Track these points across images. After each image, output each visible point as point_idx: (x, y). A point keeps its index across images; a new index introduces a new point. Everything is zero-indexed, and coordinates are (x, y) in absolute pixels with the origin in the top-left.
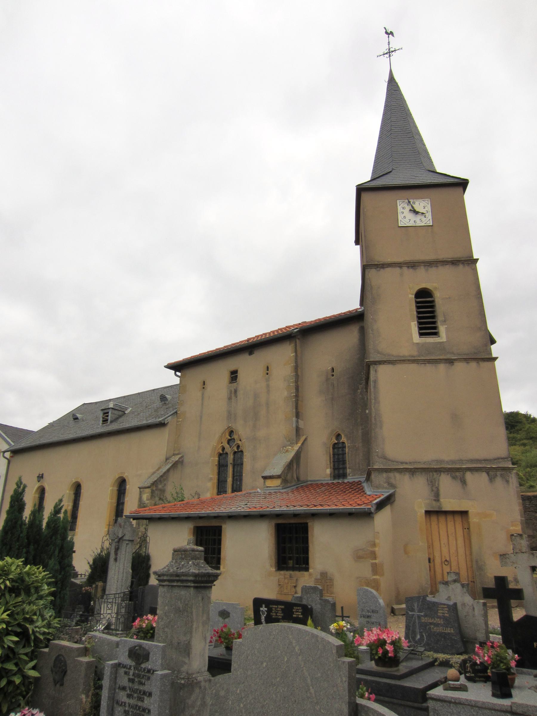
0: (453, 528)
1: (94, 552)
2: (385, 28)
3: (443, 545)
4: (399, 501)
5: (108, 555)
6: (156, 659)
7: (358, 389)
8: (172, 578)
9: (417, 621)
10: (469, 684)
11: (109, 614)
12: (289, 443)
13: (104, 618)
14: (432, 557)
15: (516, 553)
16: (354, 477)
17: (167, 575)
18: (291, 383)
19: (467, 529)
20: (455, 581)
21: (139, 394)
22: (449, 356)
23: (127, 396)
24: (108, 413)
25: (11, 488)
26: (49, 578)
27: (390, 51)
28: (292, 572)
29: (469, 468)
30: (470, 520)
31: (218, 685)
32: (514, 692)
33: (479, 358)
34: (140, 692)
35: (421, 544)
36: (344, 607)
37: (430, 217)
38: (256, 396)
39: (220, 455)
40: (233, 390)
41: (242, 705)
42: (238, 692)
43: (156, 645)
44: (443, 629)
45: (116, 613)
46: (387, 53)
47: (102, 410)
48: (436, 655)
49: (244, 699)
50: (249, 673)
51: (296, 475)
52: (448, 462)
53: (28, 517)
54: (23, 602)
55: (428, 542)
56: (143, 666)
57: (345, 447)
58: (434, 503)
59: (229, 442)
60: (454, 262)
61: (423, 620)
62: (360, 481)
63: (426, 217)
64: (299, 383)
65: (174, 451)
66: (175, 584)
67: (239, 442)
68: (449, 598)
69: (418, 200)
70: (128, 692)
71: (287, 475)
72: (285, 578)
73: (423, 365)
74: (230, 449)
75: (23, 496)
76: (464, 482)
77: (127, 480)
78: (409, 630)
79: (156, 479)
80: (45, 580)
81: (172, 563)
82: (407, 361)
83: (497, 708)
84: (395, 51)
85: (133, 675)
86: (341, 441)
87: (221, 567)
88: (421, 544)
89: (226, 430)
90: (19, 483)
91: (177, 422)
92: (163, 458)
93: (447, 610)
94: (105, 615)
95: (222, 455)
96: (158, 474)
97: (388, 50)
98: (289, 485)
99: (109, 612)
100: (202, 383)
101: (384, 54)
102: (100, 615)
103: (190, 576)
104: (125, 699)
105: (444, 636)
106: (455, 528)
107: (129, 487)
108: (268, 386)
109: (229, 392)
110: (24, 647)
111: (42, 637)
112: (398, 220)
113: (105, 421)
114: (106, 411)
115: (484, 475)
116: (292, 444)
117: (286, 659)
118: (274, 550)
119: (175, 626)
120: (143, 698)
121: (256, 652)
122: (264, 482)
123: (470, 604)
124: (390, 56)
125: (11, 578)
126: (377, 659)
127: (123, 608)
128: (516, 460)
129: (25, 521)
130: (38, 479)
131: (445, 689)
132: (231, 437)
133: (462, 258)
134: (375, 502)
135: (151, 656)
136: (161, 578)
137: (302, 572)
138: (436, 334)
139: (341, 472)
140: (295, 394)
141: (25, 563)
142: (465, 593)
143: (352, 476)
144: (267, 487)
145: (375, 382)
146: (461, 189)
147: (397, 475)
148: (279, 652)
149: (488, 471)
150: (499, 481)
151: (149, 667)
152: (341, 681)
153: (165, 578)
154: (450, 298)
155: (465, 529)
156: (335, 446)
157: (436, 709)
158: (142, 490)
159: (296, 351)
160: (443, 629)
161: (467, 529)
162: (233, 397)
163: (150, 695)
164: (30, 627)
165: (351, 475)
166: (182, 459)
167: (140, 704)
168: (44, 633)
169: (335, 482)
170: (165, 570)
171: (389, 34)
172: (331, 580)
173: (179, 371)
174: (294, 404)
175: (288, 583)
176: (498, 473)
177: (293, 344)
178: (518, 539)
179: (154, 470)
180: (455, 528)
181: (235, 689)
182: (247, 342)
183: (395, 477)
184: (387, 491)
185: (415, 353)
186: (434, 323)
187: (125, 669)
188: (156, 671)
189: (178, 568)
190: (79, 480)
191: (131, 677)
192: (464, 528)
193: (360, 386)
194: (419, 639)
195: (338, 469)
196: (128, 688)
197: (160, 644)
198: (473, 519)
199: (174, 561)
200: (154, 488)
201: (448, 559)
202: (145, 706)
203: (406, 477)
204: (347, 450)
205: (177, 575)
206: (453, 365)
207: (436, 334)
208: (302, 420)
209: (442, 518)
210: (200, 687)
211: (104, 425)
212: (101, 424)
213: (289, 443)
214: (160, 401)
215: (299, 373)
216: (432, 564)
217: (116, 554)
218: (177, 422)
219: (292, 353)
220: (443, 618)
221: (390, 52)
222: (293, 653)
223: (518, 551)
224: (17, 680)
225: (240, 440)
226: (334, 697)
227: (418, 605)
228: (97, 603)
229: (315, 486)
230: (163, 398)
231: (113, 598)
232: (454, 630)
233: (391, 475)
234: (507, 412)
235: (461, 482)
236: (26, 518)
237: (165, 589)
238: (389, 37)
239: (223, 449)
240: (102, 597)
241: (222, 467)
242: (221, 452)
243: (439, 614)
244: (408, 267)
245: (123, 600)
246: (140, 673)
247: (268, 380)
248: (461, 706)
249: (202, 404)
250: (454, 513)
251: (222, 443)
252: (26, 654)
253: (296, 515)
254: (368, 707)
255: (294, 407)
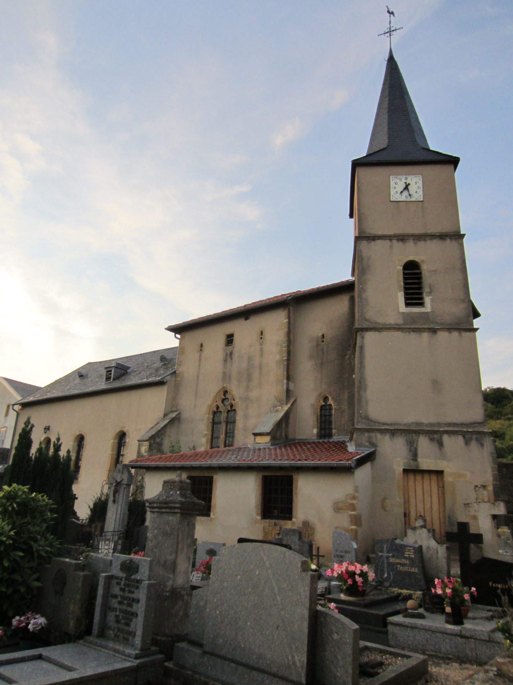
0: (429, 487)
1: (94, 497)
2: (387, 7)
3: (418, 501)
4: (379, 460)
5: (107, 501)
6: (144, 571)
7: (346, 354)
8: (161, 505)
9: (385, 561)
10: (426, 614)
11: (106, 549)
12: (279, 403)
13: (102, 553)
14: (407, 512)
15: (479, 502)
16: (339, 437)
17: (157, 503)
18: (283, 348)
19: (441, 488)
20: (422, 527)
21: (141, 355)
22: (432, 326)
23: (130, 356)
24: (111, 371)
25: (21, 426)
26: (52, 504)
27: (391, 30)
28: (276, 521)
29: (447, 431)
30: (445, 479)
31: (198, 597)
32: (465, 621)
33: (462, 329)
34: (129, 600)
35: (398, 499)
36: (320, 548)
37: (421, 193)
38: (250, 359)
39: (214, 413)
40: (229, 353)
41: (218, 612)
42: (215, 601)
43: (145, 560)
44: (408, 569)
45: (113, 549)
46: (387, 33)
47: (106, 368)
48: (400, 591)
49: (220, 607)
50: (225, 584)
51: (285, 432)
52: (427, 425)
53: (34, 454)
54: (28, 523)
55: (405, 498)
56: (133, 577)
57: (332, 409)
58: (412, 462)
59: (223, 401)
60: (442, 237)
61: (392, 560)
62: (344, 441)
63: (417, 193)
64: (291, 348)
65: (172, 408)
66: (164, 510)
67: (233, 402)
68: (416, 542)
69: (410, 176)
70: (119, 599)
71: (276, 433)
72: (269, 526)
73: (408, 333)
74: (224, 408)
75: (31, 435)
76: (441, 444)
77: (127, 434)
78: (378, 569)
79: (154, 433)
80: (49, 506)
81: (162, 493)
82: (393, 329)
83: (448, 632)
84: (396, 30)
85: (124, 585)
86: (328, 403)
87: (211, 514)
88: (398, 499)
89: (221, 389)
90: (28, 423)
91: (176, 381)
92: (161, 414)
93: (413, 552)
94: (103, 550)
95: (216, 413)
96: (156, 429)
97: (389, 29)
98: (278, 442)
99: (106, 547)
100: (200, 345)
101: (385, 33)
102: (97, 550)
103: (177, 503)
104: (116, 605)
105: (409, 574)
106: (431, 486)
107: (129, 441)
108: (261, 350)
109: (225, 355)
110: (29, 562)
111: (44, 554)
112: (390, 195)
113: (108, 378)
114: (109, 369)
115: (460, 438)
116: (281, 405)
117: (257, 573)
118: (261, 499)
119: (163, 547)
120: (132, 604)
121: (232, 567)
122: (255, 439)
123: (435, 548)
124: (390, 35)
125: (18, 502)
126: (345, 589)
127: (119, 544)
128: (500, 433)
129: (32, 457)
130: (44, 431)
131: (405, 616)
132: (225, 396)
133: (450, 233)
134: (355, 458)
135: (140, 569)
136: (152, 505)
137: (285, 521)
138: (422, 304)
139: (327, 431)
140: (286, 358)
141: (32, 491)
142: (431, 537)
143: (337, 436)
144: (257, 443)
145: (362, 348)
146: (452, 167)
147: (379, 436)
148: (252, 566)
149: (464, 434)
150: (474, 444)
151: (138, 578)
152: (304, 591)
153: (155, 505)
154: (436, 271)
155: (440, 487)
156: (322, 408)
157: (395, 632)
158: (140, 443)
159: (289, 318)
160: (408, 569)
161: (442, 487)
162: (229, 360)
163: (138, 601)
164: (35, 546)
165: (336, 435)
166: (179, 416)
167: (129, 609)
168: (47, 552)
169: (321, 441)
170: (156, 498)
171: (391, 13)
172: (313, 529)
173: (179, 334)
174: (286, 367)
175: (272, 530)
176: (474, 437)
177: (286, 312)
178: (481, 490)
179: (153, 425)
180: (431, 486)
181: (212, 599)
182: (243, 308)
183: (376, 437)
184: (368, 449)
185: (400, 321)
186: (421, 294)
187: (116, 580)
188: (144, 581)
189: (167, 497)
190: (82, 433)
191: (122, 586)
192: (438, 486)
193: (349, 352)
194: (386, 577)
195: (325, 429)
196: (119, 596)
197: (147, 559)
198: (448, 479)
199: (164, 491)
200: (152, 442)
201: (423, 515)
202: (133, 611)
203: (387, 437)
204: (333, 412)
205: (166, 503)
206: (436, 334)
207: (422, 304)
208: (293, 382)
209: (419, 477)
210: (183, 600)
211: (107, 382)
212: (104, 382)
213: (279, 403)
214: (160, 362)
215: (292, 339)
216: (407, 519)
217: (114, 496)
218: (176, 381)
219: (285, 319)
220: (409, 559)
221: (390, 32)
222: (264, 567)
223: (480, 501)
224: (23, 589)
225: (234, 400)
226: (298, 604)
227: (387, 547)
228: (96, 540)
229: (303, 443)
230: (163, 359)
231: (110, 536)
232: (418, 570)
233: (373, 434)
234: (494, 388)
235: (438, 443)
236: (33, 454)
237: (155, 515)
238: (390, 16)
239: (218, 407)
240: (101, 535)
241: (214, 423)
242: (216, 410)
243: (405, 555)
244: (398, 240)
245: (119, 538)
246: (130, 583)
247: (261, 344)
248: (417, 630)
249: (200, 365)
250: (430, 472)
251: (217, 402)
252: (31, 568)
253: (281, 468)
254: (326, 613)
255: (286, 370)
